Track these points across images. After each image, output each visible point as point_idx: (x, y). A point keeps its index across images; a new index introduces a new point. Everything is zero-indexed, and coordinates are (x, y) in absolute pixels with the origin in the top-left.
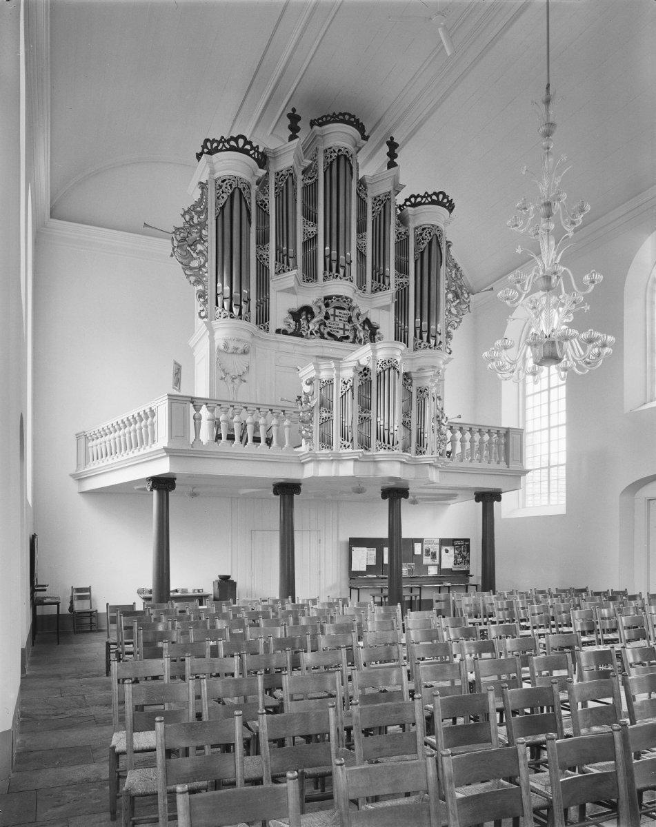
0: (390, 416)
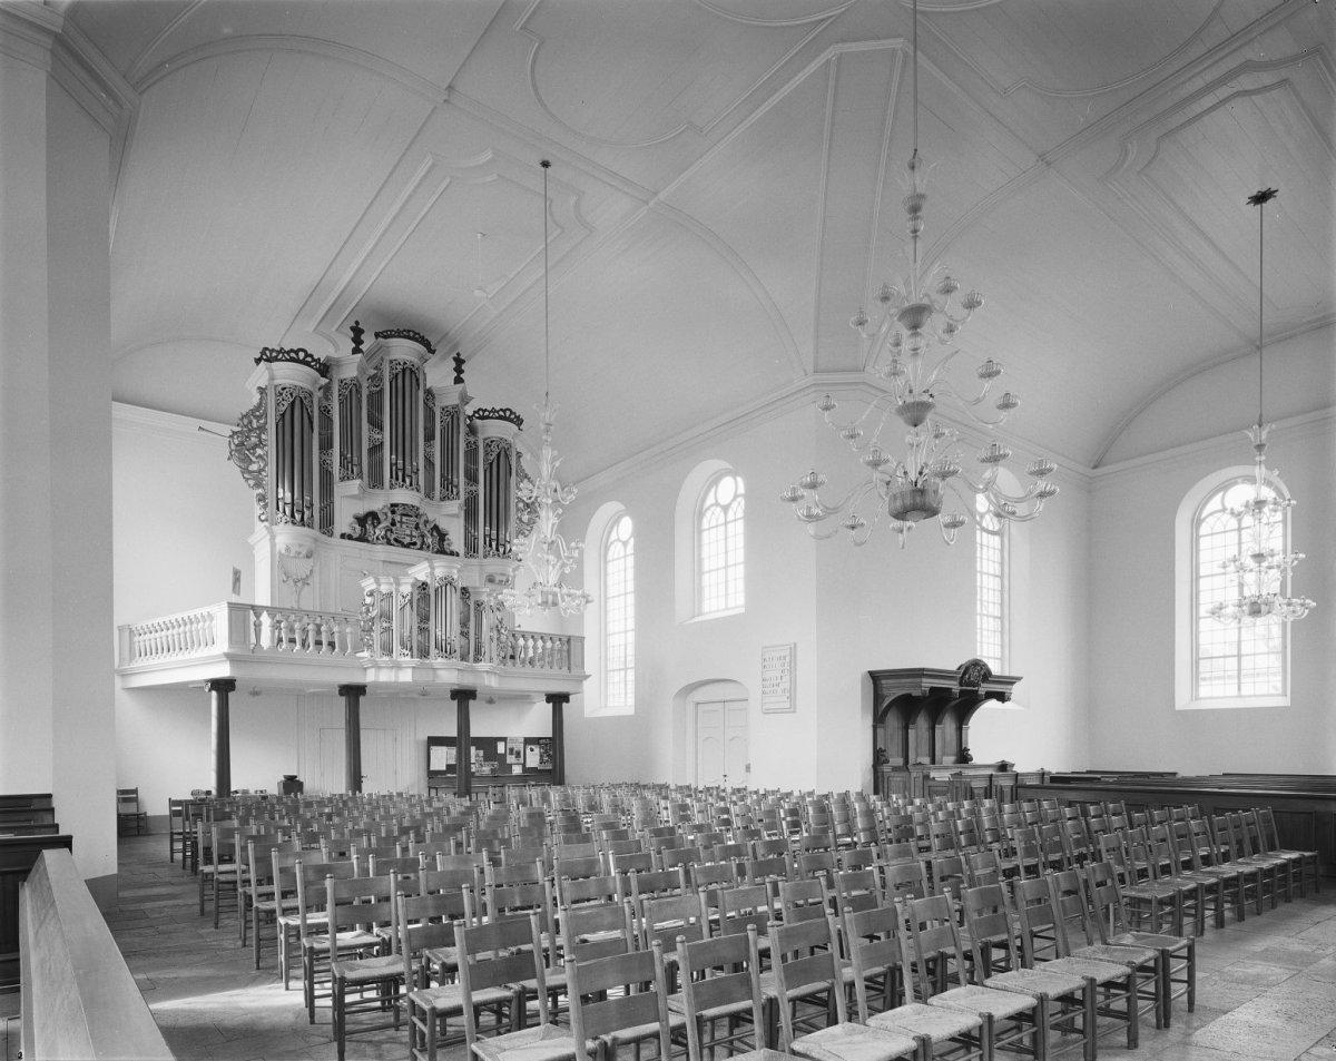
0: (447, 624)
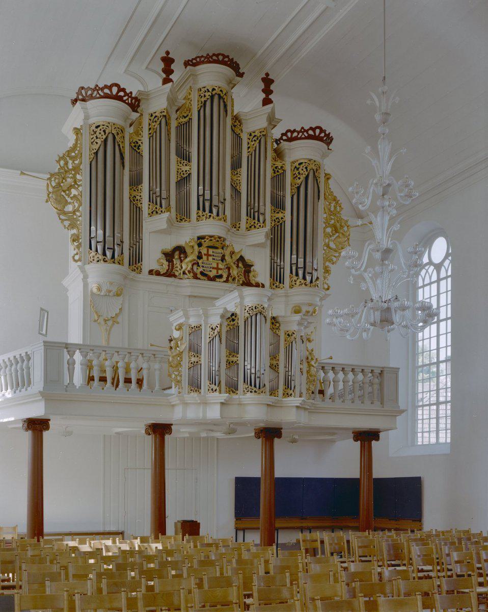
0: (255, 359)
